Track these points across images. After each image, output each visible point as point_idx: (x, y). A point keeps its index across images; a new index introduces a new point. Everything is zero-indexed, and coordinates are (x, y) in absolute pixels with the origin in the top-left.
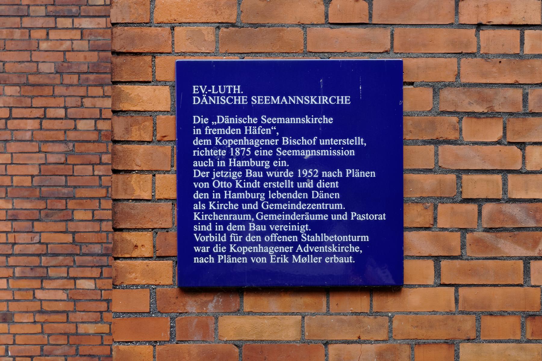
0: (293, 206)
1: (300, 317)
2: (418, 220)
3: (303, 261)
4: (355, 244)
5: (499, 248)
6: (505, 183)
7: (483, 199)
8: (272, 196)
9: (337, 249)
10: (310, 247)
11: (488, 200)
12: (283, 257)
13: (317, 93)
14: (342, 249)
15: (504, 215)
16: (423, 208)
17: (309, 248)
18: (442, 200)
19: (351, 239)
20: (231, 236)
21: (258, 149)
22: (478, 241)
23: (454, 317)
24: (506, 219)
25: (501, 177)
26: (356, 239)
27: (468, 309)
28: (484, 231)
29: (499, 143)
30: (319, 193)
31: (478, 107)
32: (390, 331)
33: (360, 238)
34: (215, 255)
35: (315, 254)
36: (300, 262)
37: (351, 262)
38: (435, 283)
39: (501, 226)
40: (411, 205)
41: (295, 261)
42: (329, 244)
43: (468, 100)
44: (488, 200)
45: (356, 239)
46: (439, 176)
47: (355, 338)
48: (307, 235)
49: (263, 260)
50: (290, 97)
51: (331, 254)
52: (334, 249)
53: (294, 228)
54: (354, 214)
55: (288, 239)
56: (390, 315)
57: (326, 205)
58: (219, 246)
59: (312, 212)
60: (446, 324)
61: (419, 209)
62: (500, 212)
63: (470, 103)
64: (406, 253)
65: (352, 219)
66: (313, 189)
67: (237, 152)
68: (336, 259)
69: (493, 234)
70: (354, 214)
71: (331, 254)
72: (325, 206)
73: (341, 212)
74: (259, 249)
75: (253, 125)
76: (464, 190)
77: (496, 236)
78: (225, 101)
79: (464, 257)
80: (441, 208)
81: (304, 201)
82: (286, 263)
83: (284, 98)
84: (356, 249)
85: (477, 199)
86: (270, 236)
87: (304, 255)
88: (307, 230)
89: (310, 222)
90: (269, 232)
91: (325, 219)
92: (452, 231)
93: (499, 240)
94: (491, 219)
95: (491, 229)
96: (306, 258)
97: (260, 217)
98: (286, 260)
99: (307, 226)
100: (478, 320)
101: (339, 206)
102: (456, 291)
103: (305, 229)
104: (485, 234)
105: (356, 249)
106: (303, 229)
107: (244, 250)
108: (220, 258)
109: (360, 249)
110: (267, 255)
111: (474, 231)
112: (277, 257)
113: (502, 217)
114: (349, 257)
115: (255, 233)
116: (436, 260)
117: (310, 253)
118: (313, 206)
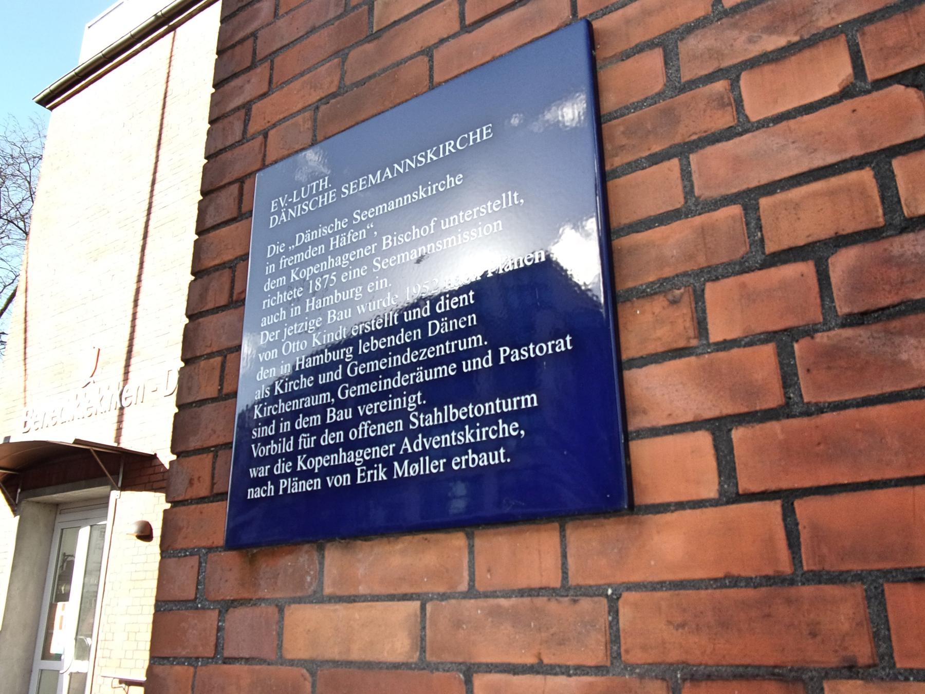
0: (399, 360)
1: (417, 604)
2: (659, 333)
3: (412, 474)
4: (508, 417)
5: (905, 364)
6: (886, 184)
7: (825, 243)
8: (363, 349)
9: (474, 435)
10: (425, 440)
11: (841, 241)
12: (378, 468)
13: (436, 142)
14: (484, 433)
15: (900, 266)
16: (666, 303)
17: (423, 442)
18: (714, 273)
19: (501, 407)
20: (300, 440)
21: (347, 270)
22: (831, 354)
23: (793, 591)
24: (909, 277)
25: (872, 173)
26: (510, 405)
27: (834, 565)
28: (843, 326)
29: (846, 93)
30: (440, 322)
31: (774, 37)
32: (614, 637)
33: (519, 402)
34: (275, 480)
35: (434, 454)
36: (406, 475)
37: (503, 461)
38: (722, 492)
39: (895, 299)
40: (636, 304)
41: (397, 474)
42: (459, 425)
43: (743, 38)
44: (841, 241)
45: (510, 405)
46: (698, 220)
47: (530, 660)
48: (419, 414)
49: (345, 479)
50: (396, 166)
51: (462, 449)
52: (468, 436)
53: (396, 403)
54: (505, 351)
55: (384, 428)
56: (610, 592)
57: (453, 344)
58: (282, 462)
59: (429, 364)
60: (769, 615)
61: (657, 310)
62: (888, 260)
63: (751, 41)
64: (635, 423)
65: (502, 362)
66: (429, 318)
67: (318, 284)
68: (473, 459)
69: (874, 327)
70: (505, 351)
71: (462, 449)
72: (450, 346)
73: (479, 352)
74: (341, 458)
75: (343, 230)
76: (768, 233)
77: (887, 332)
78: (308, 207)
79: (797, 410)
80: (712, 291)
81: (415, 345)
82: (383, 481)
83: (387, 170)
84: (510, 430)
85: (808, 245)
86: (357, 428)
87: (414, 458)
88: (419, 403)
89: (424, 387)
90: (356, 420)
91: (452, 373)
92: (750, 344)
93: (897, 340)
94: (859, 281)
95: (864, 314)
96: (416, 466)
97: (343, 394)
98: (382, 476)
99: (419, 394)
100: (876, 600)
101: (477, 340)
102: (788, 513)
103: (416, 402)
104: (848, 332)
105: (510, 430)
106: (412, 402)
107: (319, 462)
108: (283, 483)
109: (520, 428)
110: (350, 468)
111: (817, 331)
112: (368, 469)
113: (894, 274)
114: (498, 450)
115: (335, 427)
116: (719, 429)
117: (424, 452)
118: (428, 353)
